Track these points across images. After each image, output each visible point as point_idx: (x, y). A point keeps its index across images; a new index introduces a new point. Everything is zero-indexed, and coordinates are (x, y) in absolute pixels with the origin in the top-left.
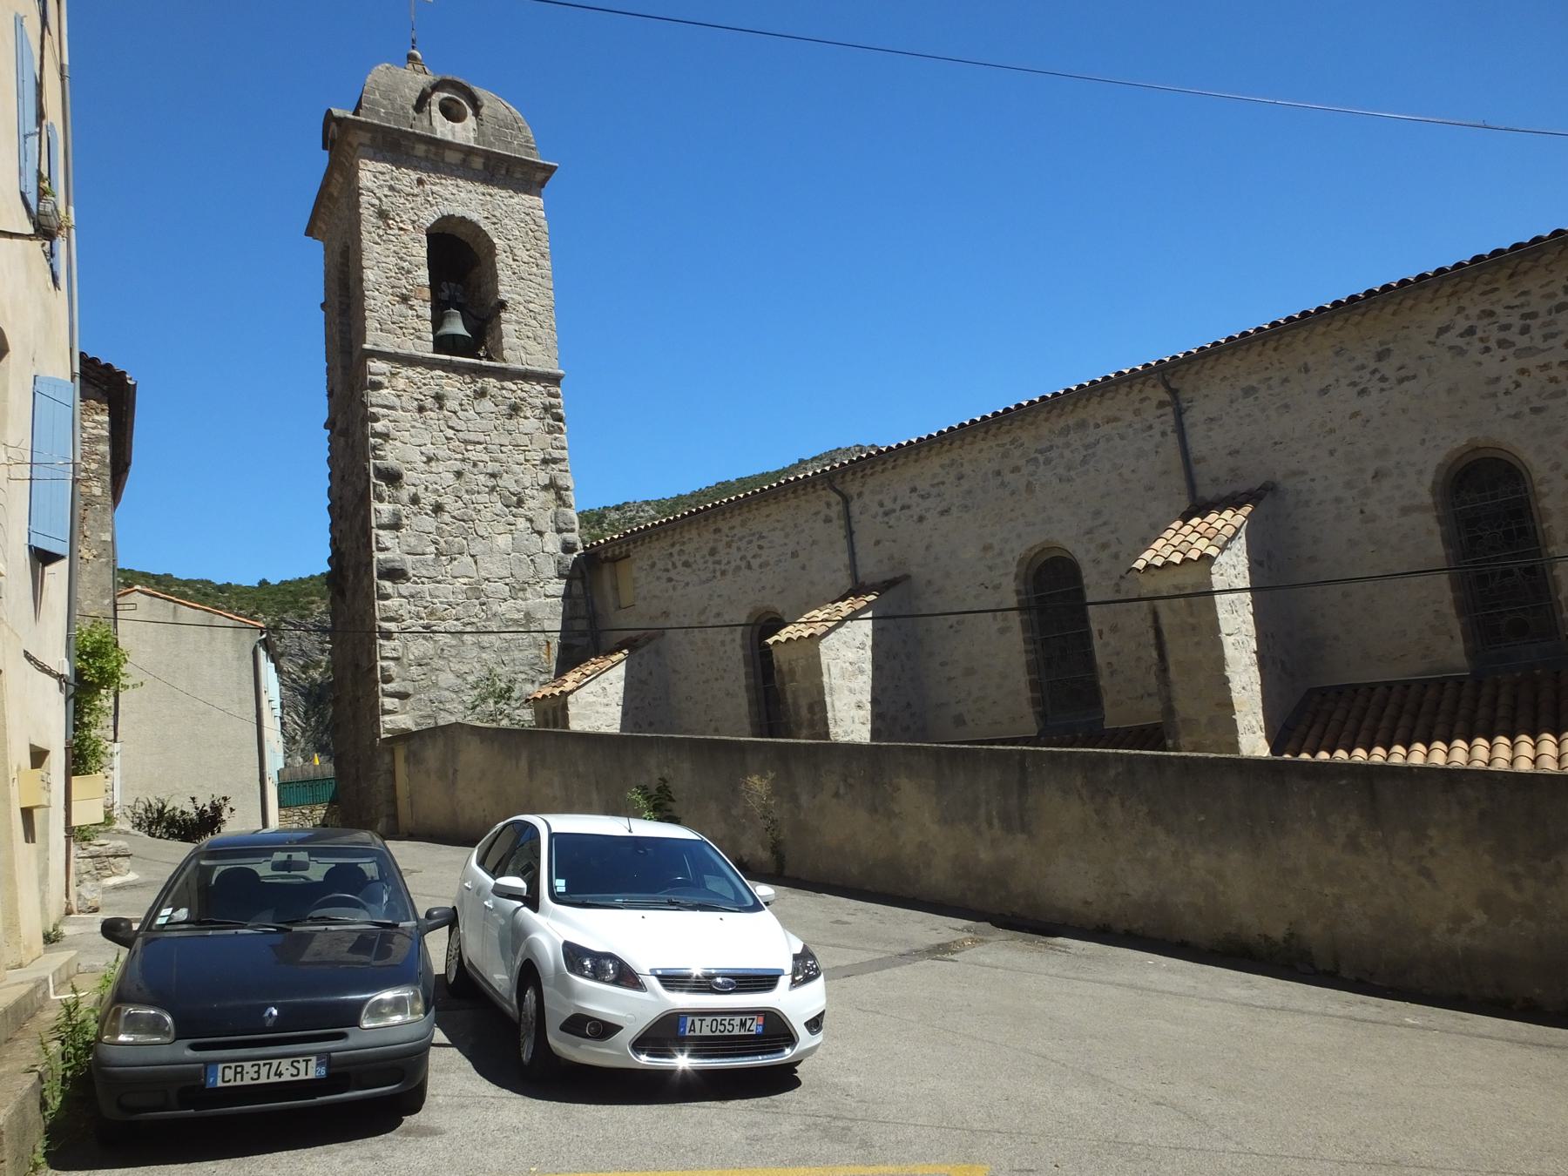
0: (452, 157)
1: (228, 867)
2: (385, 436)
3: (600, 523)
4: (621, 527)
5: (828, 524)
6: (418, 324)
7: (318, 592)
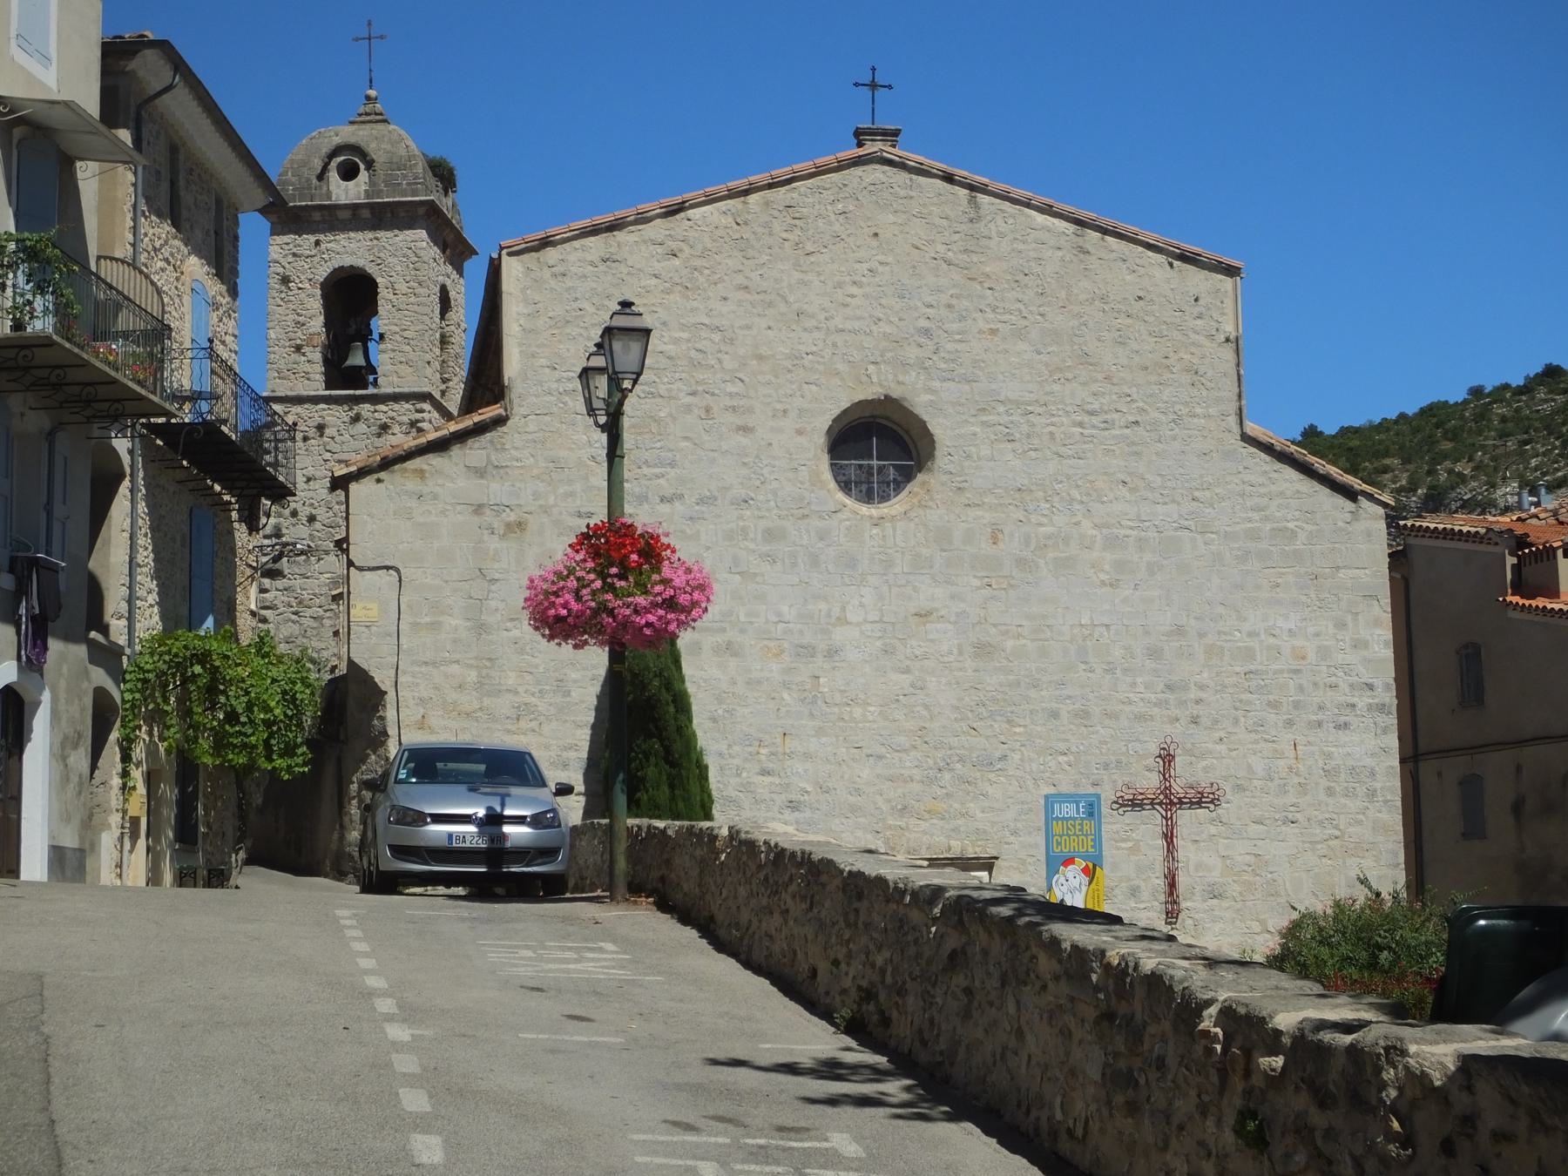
6: (308, 367)
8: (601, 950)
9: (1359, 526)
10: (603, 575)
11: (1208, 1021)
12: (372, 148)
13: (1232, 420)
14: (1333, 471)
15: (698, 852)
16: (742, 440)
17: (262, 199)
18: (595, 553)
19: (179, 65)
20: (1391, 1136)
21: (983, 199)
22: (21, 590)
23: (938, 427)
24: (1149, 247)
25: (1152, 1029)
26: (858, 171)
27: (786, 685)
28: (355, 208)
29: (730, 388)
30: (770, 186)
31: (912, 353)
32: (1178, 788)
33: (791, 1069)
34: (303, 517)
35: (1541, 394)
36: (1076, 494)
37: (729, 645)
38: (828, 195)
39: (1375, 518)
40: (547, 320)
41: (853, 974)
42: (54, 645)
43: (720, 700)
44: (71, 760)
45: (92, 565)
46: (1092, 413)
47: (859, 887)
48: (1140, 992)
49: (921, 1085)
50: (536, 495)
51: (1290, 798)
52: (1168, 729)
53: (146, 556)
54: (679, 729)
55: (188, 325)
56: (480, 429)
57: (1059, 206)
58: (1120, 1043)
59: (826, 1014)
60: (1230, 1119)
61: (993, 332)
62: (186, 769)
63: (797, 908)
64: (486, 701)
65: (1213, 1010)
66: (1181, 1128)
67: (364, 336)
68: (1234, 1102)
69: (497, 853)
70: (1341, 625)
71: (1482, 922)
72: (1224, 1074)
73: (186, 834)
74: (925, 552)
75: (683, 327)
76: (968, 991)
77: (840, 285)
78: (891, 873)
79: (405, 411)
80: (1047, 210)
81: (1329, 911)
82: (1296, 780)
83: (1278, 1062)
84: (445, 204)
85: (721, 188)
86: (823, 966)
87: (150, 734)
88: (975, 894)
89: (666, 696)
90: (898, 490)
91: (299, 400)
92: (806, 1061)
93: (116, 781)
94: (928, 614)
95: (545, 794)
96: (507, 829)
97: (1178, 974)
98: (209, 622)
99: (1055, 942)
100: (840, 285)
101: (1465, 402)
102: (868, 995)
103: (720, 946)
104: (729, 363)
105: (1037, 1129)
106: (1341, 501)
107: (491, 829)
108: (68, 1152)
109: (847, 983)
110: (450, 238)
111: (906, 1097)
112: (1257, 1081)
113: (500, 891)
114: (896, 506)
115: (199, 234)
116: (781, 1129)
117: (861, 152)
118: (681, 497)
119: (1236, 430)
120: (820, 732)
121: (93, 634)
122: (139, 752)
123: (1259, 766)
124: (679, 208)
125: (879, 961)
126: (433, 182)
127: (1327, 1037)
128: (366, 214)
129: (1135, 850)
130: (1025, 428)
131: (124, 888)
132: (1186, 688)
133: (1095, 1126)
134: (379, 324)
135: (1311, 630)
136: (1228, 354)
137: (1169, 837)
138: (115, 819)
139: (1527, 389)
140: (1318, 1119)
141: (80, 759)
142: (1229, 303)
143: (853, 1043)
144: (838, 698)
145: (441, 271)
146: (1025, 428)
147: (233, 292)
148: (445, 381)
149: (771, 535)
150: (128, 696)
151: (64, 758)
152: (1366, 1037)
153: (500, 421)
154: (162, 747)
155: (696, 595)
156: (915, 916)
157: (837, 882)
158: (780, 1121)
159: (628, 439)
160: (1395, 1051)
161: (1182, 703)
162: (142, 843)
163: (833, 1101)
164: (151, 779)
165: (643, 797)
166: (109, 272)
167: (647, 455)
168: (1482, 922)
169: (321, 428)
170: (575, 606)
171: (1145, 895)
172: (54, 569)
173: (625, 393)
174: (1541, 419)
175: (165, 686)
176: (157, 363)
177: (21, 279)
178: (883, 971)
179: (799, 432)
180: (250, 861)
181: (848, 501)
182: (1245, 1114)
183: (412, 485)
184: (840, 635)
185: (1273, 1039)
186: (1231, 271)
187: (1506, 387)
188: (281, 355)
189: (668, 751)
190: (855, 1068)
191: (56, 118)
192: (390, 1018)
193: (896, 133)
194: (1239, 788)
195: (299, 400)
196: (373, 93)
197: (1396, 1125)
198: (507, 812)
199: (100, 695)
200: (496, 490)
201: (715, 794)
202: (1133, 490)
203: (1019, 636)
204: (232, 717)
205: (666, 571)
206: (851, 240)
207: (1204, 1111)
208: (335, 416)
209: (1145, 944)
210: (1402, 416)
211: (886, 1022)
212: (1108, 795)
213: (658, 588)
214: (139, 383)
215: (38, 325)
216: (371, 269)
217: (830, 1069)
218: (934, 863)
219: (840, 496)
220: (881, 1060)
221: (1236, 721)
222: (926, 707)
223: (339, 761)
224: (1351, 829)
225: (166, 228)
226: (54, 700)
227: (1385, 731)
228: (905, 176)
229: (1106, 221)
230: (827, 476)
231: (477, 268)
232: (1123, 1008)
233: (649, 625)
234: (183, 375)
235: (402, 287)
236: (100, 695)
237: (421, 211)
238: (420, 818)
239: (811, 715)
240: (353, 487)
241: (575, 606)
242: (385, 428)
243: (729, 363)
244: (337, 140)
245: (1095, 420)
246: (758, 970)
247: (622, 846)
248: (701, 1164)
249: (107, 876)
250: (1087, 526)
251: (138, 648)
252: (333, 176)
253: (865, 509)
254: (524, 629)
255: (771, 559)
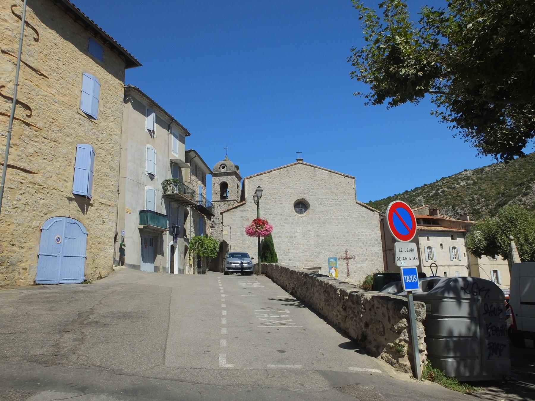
0: (223, 174)
1: (432, 290)
2: (213, 211)
3: (481, 172)
4: (490, 173)
5: (300, 212)
6: (218, 196)
7: (384, 203)
8: (256, 282)
9: (375, 216)
10: (256, 226)
11: (338, 292)
12: (227, 164)
13: (355, 200)
14: (371, 208)
15: (271, 267)
16: (281, 205)
17: (209, 172)
18: (255, 223)
19: (196, 154)
20: (362, 308)
21: (316, 169)
22: (174, 230)
23: (310, 203)
24: (341, 175)
25: (331, 293)
26: (297, 165)
27: (288, 242)
28: (224, 173)
29: (279, 198)
30: (284, 168)
31: (306, 192)
32: (348, 256)
33: (281, 300)
34: (217, 218)
35: (405, 195)
36: (331, 212)
37: (280, 236)
38: (293, 169)
39: (377, 214)
40: (106, 213)
41: (292, 285)
42: (178, 238)
43: (279, 245)
44: (181, 256)
45: (184, 227)
46: (333, 200)
47: (292, 272)
48: (329, 287)
49: (300, 302)
50: (250, 215)
51: (366, 257)
52: (347, 247)
53: (192, 225)
54: (272, 249)
55: (198, 191)
56: (242, 205)
57: (327, 169)
58: (327, 295)
59: (287, 291)
60: (341, 306)
61: (318, 188)
62: (199, 257)
63: (284, 276)
64: (244, 246)
65: (339, 290)
66: (335, 308)
67: (226, 192)
68: (342, 304)
69: (242, 268)
70: (373, 231)
71: (379, 276)
72: (340, 300)
73: (199, 266)
74: (309, 221)
75: (272, 189)
76: (307, 288)
77: (295, 182)
78: (296, 270)
79: (232, 202)
80: (326, 170)
81: (373, 275)
82: (367, 254)
83: (347, 297)
84: (238, 172)
85: (277, 168)
86: (288, 284)
87: (193, 251)
88: (308, 273)
89: (270, 244)
90: (305, 212)
91: (217, 201)
92: (284, 299)
93: (188, 259)
94: (310, 231)
95: (250, 259)
96: (244, 265)
97: (334, 284)
98: (202, 235)
99: (318, 280)
100: (295, 182)
101: (394, 196)
102: (294, 289)
103: (274, 281)
104: (279, 194)
105: (316, 308)
106: (372, 212)
107: (242, 265)
108: (171, 314)
109: (291, 287)
110: (238, 177)
111: (298, 304)
112: (345, 300)
113: (245, 274)
114: (304, 215)
115: (200, 178)
116: (278, 309)
117: (298, 162)
118: (272, 214)
119: (355, 202)
120: (294, 249)
121: (184, 237)
122: (192, 254)
123: (361, 252)
124: (271, 171)
125: (295, 283)
126: (236, 169)
127: (353, 293)
128: (226, 174)
129: (342, 266)
130: (323, 202)
131: (190, 275)
132: (349, 241)
133: (324, 308)
134: (228, 190)
135: (368, 232)
136: (354, 190)
137: (347, 264)
138: (188, 264)
139: (403, 194)
140: (353, 306)
141: (183, 255)
142: (353, 183)
143: (291, 296)
144: (296, 243)
145: (238, 182)
146: (323, 202)
147: (205, 186)
148: (238, 198)
149: (285, 219)
150: (190, 246)
151: (180, 255)
152: (358, 293)
153: (245, 204)
154: (195, 253)
155: (270, 229)
156: (300, 276)
157: (289, 272)
158: (278, 308)
159: (260, 206)
160: (363, 295)
161: (349, 243)
162: (192, 268)
163: (286, 305)
164: (193, 258)
165: (267, 259)
166: (187, 184)
167: (267, 208)
168: (379, 276)
169: (220, 205)
170: (252, 231)
171: (344, 273)
172: (178, 227)
173: (259, 199)
174: (406, 199)
175: (195, 244)
176: (193, 197)
177: (173, 185)
178: (296, 285)
179: (289, 204)
180: (209, 270)
181: (297, 214)
182: (343, 305)
183: (232, 213)
184: (296, 234)
185: (346, 294)
186: (354, 178)
187: (400, 194)
188: (214, 195)
189: (271, 252)
190: (291, 300)
191: (178, 162)
192: (222, 293)
193: (303, 159)
194: (358, 256)
195: (217, 201)
196: (227, 156)
197: (363, 307)
198: (244, 262)
199: (186, 246)
200: (244, 214)
201: (278, 259)
202: (340, 211)
203: (323, 234)
204: (205, 249)
205: (266, 225)
206: (296, 175)
207: (338, 305)
208: (222, 203)
209: (331, 280)
210: (384, 199)
211: (296, 293)
212: (338, 257)
213: (265, 228)
214: (191, 200)
215: (176, 192)
216: (227, 182)
217: (287, 300)
218: (304, 268)
219: (296, 213)
220: (295, 298)
221: (357, 246)
222: (310, 245)
223: (222, 255)
224: (376, 262)
225: (195, 177)
226: (179, 247)
227: (380, 247)
228: (304, 166)
229: (334, 171)
230: (294, 210)
231: (242, 181)
232: (327, 290)
233: (263, 234)
234: (197, 198)
235: (231, 184)
236: (186, 246)
237: (234, 173)
238: (231, 263)
239: (292, 246)
240: (223, 214)
241: (252, 231)
242: (229, 205)
243: (279, 194)
244: (222, 163)
245: (334, 201)
246: (279, 285)
247: (260, 267)
248: (265, 314)
249: (187, 273)
250: (333, 217)
251: (191, 239)
252: (221, 168)
253: (300, 215)
254: (246, 236)
255: (286, 223)
